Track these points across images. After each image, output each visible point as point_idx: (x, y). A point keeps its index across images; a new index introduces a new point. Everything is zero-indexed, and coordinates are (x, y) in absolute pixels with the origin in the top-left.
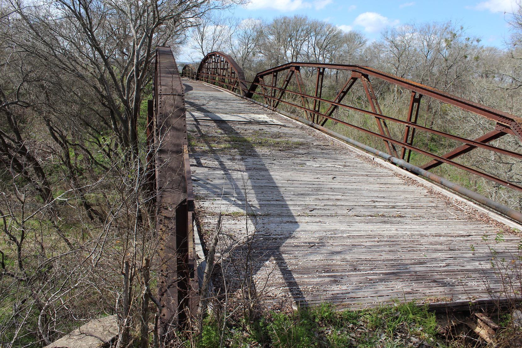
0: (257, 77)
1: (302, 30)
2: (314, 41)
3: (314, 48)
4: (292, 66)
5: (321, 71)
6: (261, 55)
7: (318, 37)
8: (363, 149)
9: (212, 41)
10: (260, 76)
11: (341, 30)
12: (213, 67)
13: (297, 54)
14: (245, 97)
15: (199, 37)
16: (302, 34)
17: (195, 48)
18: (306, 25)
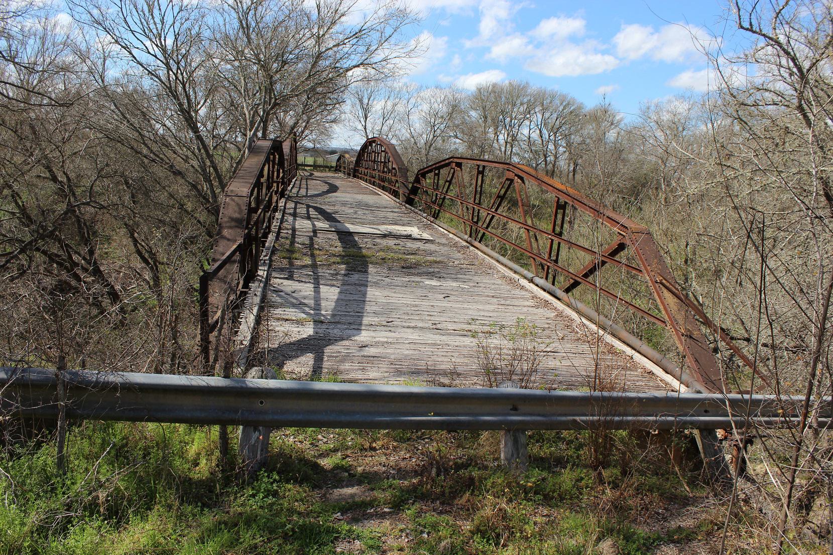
0: (417, 175)
1: (522, 104)
2: (540, 120)
3: (540, 130)
4: (452, 162)
5: (481, 169)
6: (458, 141)
7: (547, 115)
8: (511, 269)
9: (381, 120)
10: (421, 174)
11: (582, 103)
12: (383, 160)
13: (513, 140)
14: (404, 203)
15: (361, 113)
16: (521, 109)
17: (356, 129)
18: (528, 95)
